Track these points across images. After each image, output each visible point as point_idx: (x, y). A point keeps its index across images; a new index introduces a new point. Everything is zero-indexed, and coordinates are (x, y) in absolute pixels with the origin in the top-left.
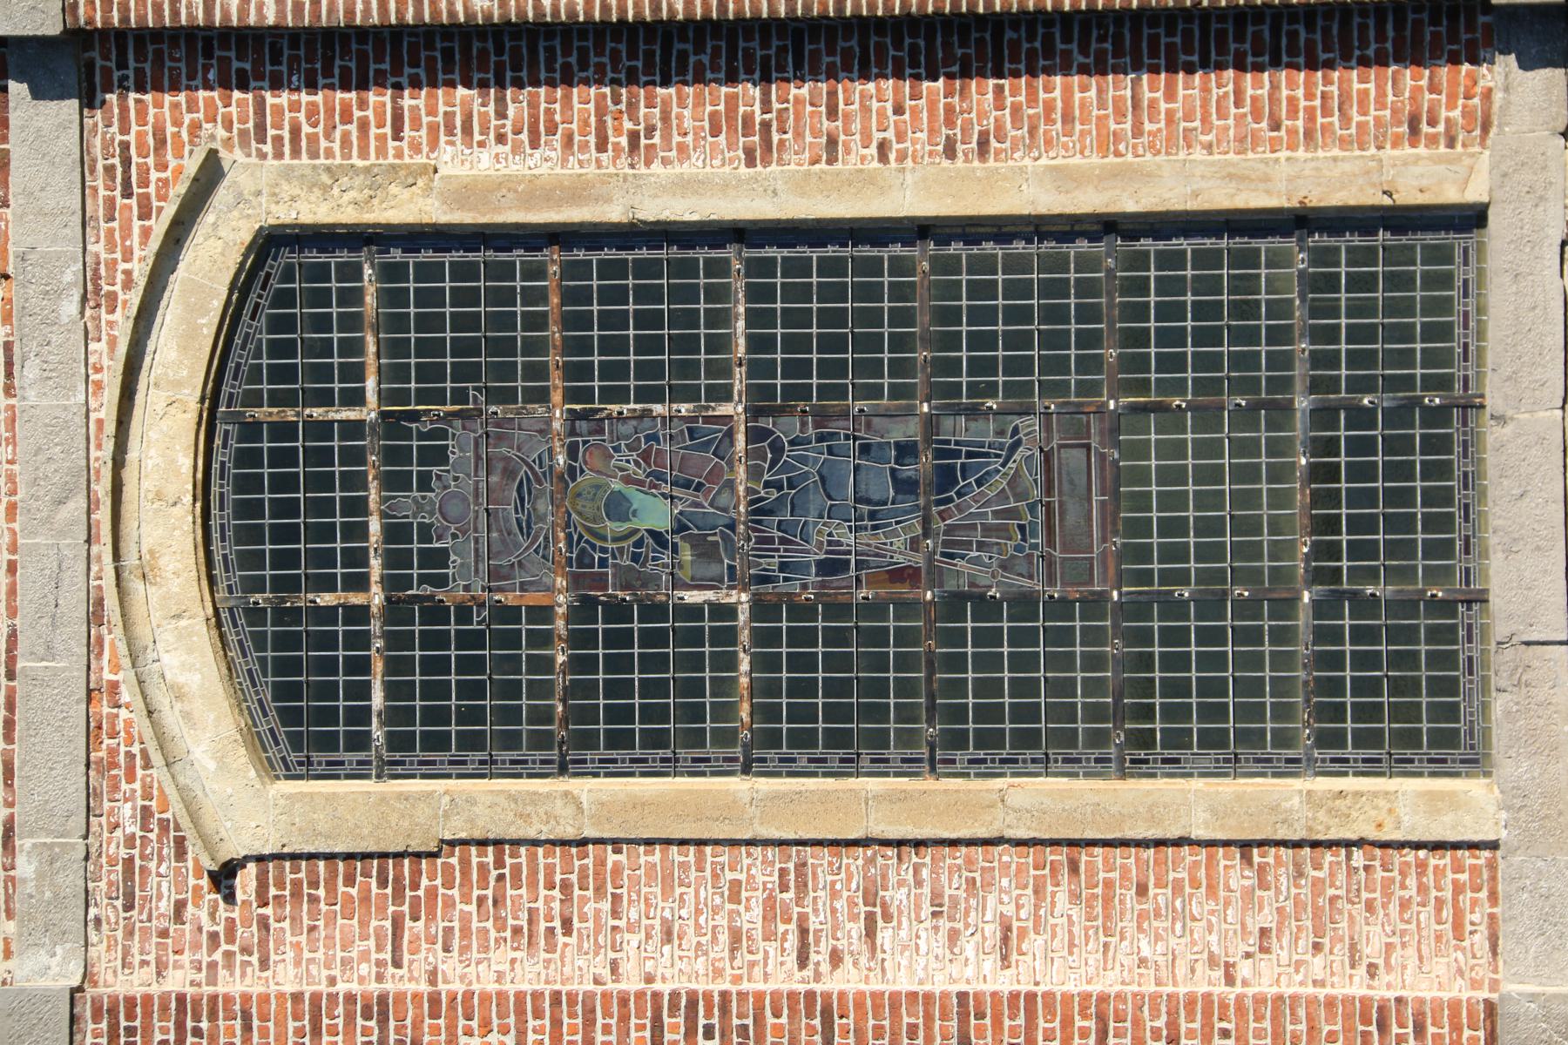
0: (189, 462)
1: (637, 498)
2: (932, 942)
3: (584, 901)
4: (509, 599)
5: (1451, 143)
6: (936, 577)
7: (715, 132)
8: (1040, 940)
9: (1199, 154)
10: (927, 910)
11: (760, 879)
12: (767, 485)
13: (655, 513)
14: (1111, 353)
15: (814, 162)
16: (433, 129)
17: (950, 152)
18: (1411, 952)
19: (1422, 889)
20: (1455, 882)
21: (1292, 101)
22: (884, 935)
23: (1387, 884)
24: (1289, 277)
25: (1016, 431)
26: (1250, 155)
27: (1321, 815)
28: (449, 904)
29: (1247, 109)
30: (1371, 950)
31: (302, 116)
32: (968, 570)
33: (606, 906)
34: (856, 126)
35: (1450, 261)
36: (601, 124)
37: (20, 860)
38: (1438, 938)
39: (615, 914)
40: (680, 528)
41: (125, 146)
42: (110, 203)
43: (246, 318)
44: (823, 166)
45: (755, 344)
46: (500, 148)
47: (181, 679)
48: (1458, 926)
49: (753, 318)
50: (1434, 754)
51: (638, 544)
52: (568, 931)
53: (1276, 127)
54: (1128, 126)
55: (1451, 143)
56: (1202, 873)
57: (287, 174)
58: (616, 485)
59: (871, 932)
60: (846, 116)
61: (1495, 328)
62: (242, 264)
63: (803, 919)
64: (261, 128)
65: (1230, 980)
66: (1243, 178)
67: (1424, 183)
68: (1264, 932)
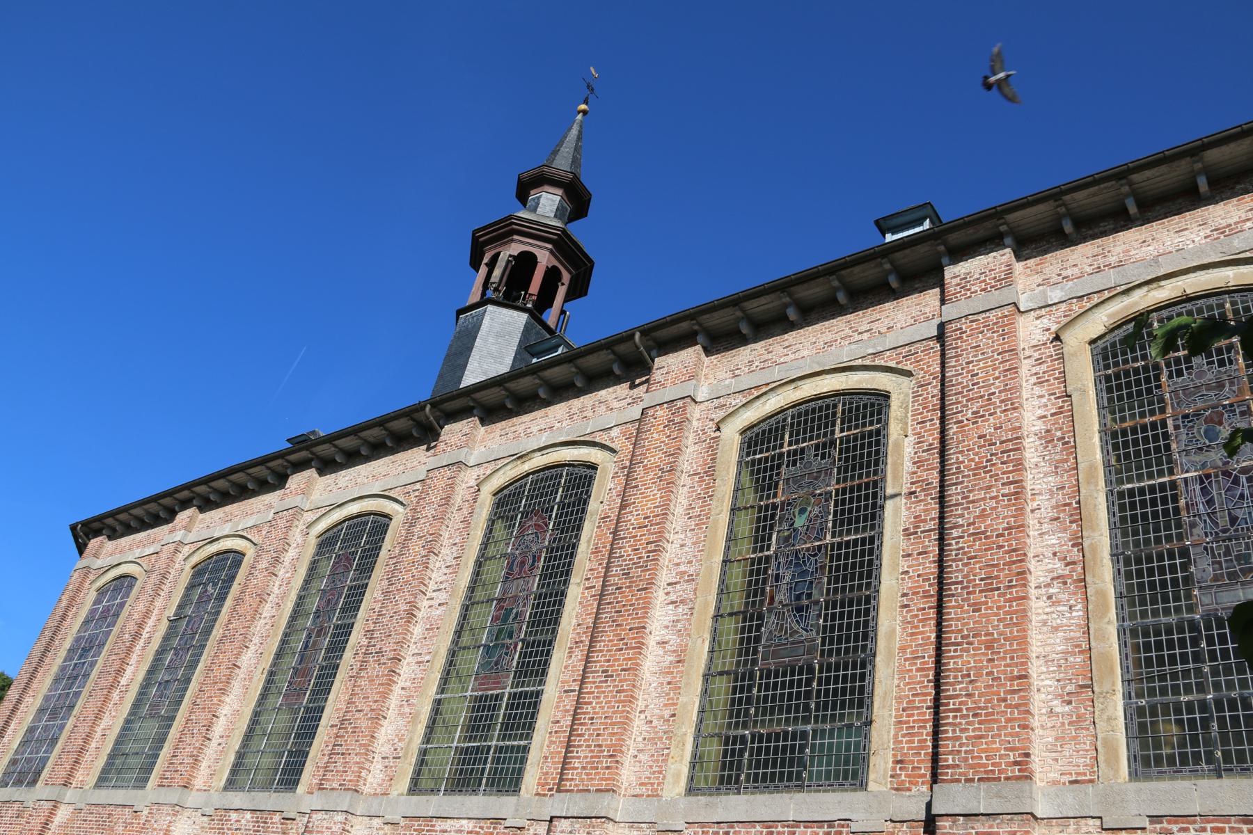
0: (825, 390)
1: (805, 516)
3: (695, 521)
5: (892, 776)
7: (915, 517)
9: (896, 682)
13: (800, 522)
14: (833, 660)
16: (920, 433)
17: (904, 595)
18: (638, 769)
19: (654, 772)
21: (912, 715)
22: (671, 607)
23: (657, 761)
25: (811, 630)
26: (894, 701)
28: (701, 486)
29: (911, 698)
30: (641, 756)
32: (771, 621)
33: (693, 527)
34: (914, 562)
35: (852, 779)
36: (919, 482)
38: (640, 778)
39: (691, 530)
40: (794, 530)
41: (917, 353)
42: (901, 353)
43: (867, 397)
46: (913, 453)
47: (768, 404)
48: (642, 784)
49: (856, 541)
51: (791, 519)
54: (908, 656)
55: (892, 776)
56: (670, 702)
57: (907, 395)
58: (809, 509)
59: (672, 603)
62: (880, 390)
63: (679, 582)
66: (884, 699)
68: (651, 722)
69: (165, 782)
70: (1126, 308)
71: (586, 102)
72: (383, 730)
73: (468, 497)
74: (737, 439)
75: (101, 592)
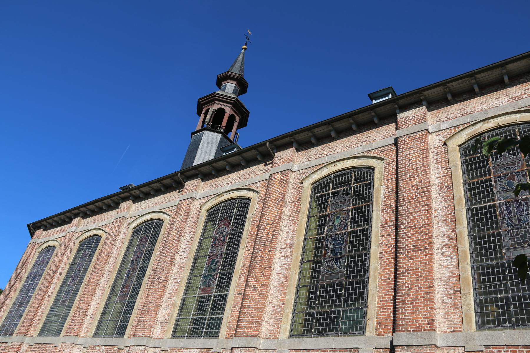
0: (347, 166)
2: (280, 264)
3: (292, 222)
4: (329, 207)
5: (376, 330)
6: (324, 260)
7: (385, 220)
8: (278, 278)
9: (378, 290)
10: (284, 263)
11: (291, 242)
12: (339, 236)
13: (337, 222)
14: (351, 280)
15: (380, 234)
16: (387, 184)
17: (381, 253)
20: (276, 333)
21: (385, 304)
22: (282, 258)
24: (359, 305)
25: (342, 268)
27: (286, 314)
30: (270, 321)
31: (389, 169)
34: (385, 239)
36: (387, 205)
37: (306, 162)
38: (270, 331)
40: (334, 226)
41: (386, 150)
44: (380, 235)
45: (357, 231)
46: (384, 193)
49: (360, 230)
50: (359, 332)
51: (333, 221)
52: (289, 221)
53: (381, 301)
55: (376, 330)
56: (282, 298)
57: (382, 168)
58: (340, 217)
59: (283, 256)
60: (386, 237)
61: (346, 338)
62: (370, 166)
63: (286, 248)
64: (388, 164)
65: (269, 303)
67: (370, 325)
68: (274, 307)
69: (68, 334)
70: (474, 131)
71: (246, 45)
72: (160, 311)
73: (196, 212)
74: (310, 187)
75: (41, 253)
